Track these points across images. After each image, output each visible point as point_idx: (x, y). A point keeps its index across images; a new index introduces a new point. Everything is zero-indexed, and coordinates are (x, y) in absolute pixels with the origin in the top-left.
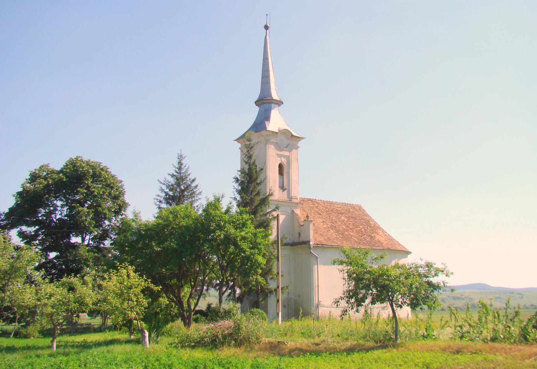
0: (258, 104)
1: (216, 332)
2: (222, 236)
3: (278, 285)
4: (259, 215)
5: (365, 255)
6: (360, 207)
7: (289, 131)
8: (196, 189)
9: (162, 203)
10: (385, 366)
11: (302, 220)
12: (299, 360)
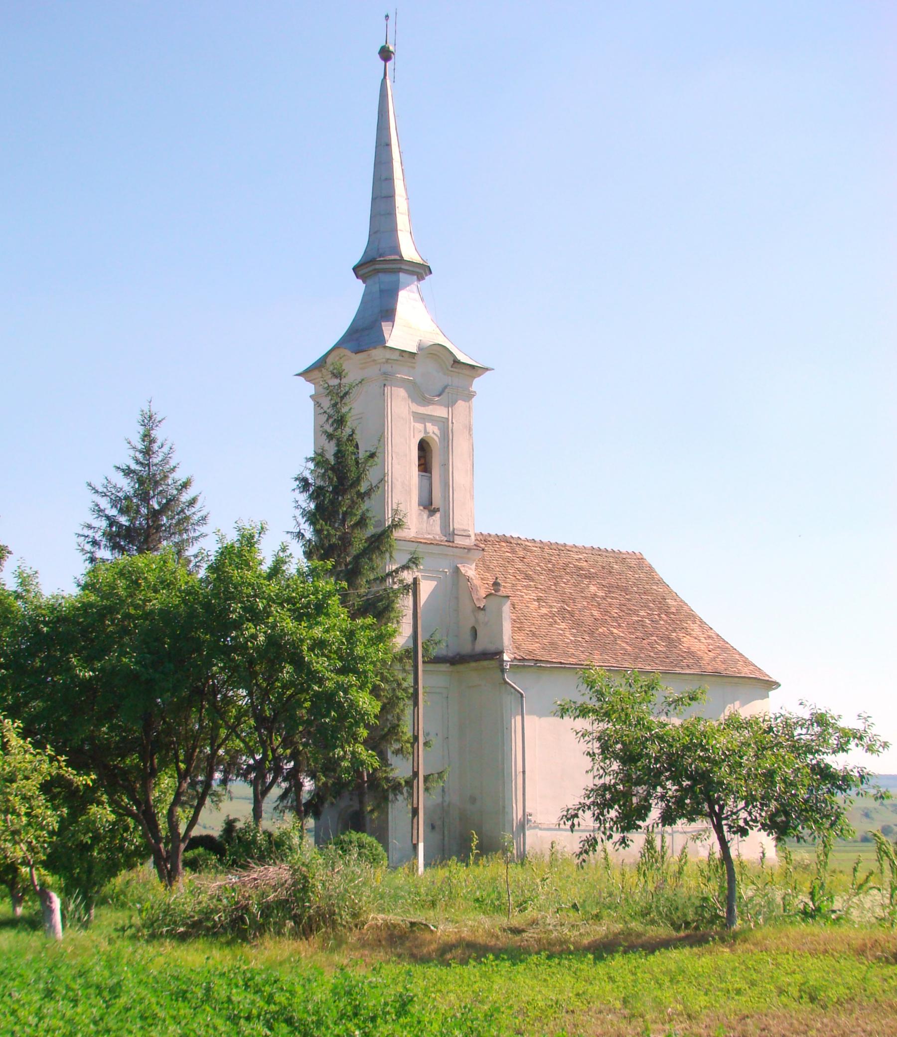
0: (361, 273)
1: (243, 896)
2: (261, 638)
3: (416, 770)
4: (365, 580)
5: (645, 692)
6: (641, 559)
7: (451, 353)
8: (193, 510)
9: (99, 548)
10: (697, 992)
11: (483, 593)
12: (465, 974)
